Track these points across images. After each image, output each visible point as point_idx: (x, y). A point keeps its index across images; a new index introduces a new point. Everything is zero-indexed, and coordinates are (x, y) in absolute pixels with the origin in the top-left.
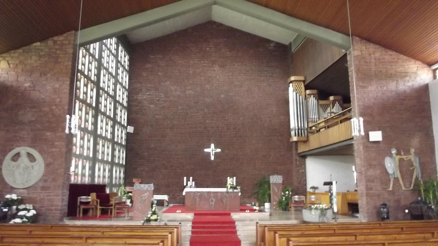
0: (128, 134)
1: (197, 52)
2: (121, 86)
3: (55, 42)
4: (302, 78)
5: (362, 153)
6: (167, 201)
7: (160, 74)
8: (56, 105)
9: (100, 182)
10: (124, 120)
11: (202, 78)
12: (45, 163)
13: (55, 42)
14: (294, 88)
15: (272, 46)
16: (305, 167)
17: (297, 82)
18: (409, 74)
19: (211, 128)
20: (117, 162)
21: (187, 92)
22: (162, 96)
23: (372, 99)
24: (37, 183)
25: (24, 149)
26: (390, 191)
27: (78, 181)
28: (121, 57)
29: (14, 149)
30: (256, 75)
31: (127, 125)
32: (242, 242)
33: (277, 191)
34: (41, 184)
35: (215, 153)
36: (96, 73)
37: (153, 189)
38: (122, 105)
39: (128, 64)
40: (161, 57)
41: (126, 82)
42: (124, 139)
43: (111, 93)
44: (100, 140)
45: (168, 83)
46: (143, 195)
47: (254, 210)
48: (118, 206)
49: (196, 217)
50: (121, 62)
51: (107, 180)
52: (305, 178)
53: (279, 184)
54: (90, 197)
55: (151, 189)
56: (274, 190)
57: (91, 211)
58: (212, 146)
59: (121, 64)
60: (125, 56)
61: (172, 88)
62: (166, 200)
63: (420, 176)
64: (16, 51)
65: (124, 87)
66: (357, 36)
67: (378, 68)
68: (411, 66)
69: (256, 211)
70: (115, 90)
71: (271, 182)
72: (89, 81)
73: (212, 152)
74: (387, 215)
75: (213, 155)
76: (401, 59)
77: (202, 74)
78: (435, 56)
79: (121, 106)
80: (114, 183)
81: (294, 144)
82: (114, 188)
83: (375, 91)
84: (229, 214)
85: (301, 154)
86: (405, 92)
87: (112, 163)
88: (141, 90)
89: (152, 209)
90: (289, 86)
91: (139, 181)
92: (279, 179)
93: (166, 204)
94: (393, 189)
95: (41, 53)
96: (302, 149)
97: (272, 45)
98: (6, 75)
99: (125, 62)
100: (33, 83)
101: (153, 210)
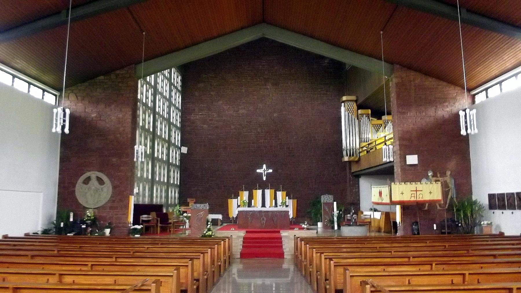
0: (182, 155)
1: (249, 70)
3: (117, 76)
6: (221, 221)
7: (212, 93)
8: (120, 134)
9: (162, 202)
13: (117, 76)
15: (326, 62)
18: (448, 100)
19: (264, 147)
21: (241, 112)
23: (411, 125)
24: (106, 203)
26: (426, 210)
30: (310, 92)
34: (109, 205)
36: (152, 99)
37: (208, 208)
38: (175, 126)
42: (178, 160)
43: (166, 116)
44: (157, 162)
49: (247, 234)
51: (163, 200)
54: (151, 216)
56: (325, 210)
57: (152, 229)
58: (264, 166)
59: (174, 86)
60: (177, 77)
61: (225, 107)
62: (220, 219)
66: (397, 64)
68: (450, 92)
69: (304, 229)
74: (418, 231)
76: (440, 85)
78: (477, 80)
80: (170, 203)
81: (348, 163)
84: (279, 232)
85: (355, 174)
87: (168, 184)
88: (194, 110)
92: (330, 199)
93: (219, 223)
95: (105, 86)
97: (326, 61)
98: (74, 107)
99: (177, 83)
101: (208, 227)
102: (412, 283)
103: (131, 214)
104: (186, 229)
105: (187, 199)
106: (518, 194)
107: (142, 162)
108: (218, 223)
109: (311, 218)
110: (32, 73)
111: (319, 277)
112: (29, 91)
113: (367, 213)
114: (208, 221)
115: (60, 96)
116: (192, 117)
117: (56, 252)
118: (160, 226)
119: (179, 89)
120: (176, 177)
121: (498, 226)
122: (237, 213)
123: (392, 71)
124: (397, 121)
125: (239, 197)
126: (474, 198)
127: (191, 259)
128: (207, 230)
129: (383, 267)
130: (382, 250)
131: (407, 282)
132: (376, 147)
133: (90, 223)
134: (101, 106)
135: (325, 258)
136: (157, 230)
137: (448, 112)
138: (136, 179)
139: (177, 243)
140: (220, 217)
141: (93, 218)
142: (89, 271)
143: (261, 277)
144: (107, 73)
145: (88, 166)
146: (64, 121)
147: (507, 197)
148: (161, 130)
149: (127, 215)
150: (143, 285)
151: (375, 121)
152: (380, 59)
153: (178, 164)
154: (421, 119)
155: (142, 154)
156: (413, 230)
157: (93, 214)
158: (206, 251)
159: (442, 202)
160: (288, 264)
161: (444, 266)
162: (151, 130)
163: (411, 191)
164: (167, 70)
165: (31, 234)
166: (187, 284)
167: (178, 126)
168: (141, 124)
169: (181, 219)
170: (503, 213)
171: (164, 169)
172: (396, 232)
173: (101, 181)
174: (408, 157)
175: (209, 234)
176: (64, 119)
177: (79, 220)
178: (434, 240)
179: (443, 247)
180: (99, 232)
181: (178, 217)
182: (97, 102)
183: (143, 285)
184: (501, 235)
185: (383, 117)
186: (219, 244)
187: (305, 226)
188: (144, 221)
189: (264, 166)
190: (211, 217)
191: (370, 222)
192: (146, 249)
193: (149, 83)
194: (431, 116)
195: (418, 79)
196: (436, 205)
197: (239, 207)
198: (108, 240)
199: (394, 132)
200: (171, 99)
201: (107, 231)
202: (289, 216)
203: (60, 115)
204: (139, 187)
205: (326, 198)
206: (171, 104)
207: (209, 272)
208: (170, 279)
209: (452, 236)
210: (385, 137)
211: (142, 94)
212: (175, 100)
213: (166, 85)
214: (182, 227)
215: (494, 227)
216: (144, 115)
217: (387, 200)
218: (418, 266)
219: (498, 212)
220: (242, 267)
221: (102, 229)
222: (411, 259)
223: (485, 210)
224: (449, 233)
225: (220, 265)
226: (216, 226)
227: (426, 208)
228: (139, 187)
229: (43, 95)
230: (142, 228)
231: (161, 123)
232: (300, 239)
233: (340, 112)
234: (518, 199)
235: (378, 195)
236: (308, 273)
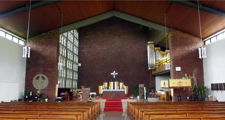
0: (79, 67)
6: (96, 95)
7: (92, 40)
8: (52, 58)
13: (51, 33)
21: (104, 48)
24: (45, 88)
25: (40, 75)
27: (60, 87)
28: (75, 34)
29: (36, 75)
31: (78, 63)
33: (142, 91)
34: (47, 88)
35: (115, 75)
37: (90, 90)
38: (76, 54)
51: (71, 86)
56: (140, 91)
57: (66, 99)
59: (75, 37)
60: (77, 33)
61: (97, 46)
64: (36, 36)
66: (172, 28)
70: (73, 49)
84: (121, 100)
85: (153, 75)
87: (73, 79)
88: (84, 47)
93: (95, 96)
94: (185, 90)
99: (77, 36)
104: (80, 99)
106: (224, 84)
107: (61, 70)
109: (134, 94)
112: (12, 40)
114: (90, 96)
115: (26, 42)
116: (83, 51)
117: (24, 109)
120: (76, 76)
121: (215, 98)
123: (170, 31)
125: (103, 85)
126: (205, 86)
127: (83, 112)
129: (166, 115)
134: (44, 46)
135: (141, 111)
138: (59, 77)
139: (77, 105)
140: (95, 93)
142: (38, 117)
144: (46, 32)
145: (38, 72)
146: (28, 52)
147: (219, 85)
148: (70, 56)
149: (55, 93)
151: (162, 52)
152: (164, 26)
156: (178, 99)
159: (191, 87)
160: (124, 114)
162: (65, 56)
165: (13, 101)
168: (61, 54)
169: (79, 94)
171: (71, 73)
172: (171, 100)
173: (43, 78)
177: (34, 95)
178: (188, 104)
179: (192, 107)
182: (42, 44)
184: (217, 101)
185: (166, 51)
186: (94, 105)
187: (132, 98)
190: (91, 93)
191: (160, 96)
193: (65, 36)
195: (181, 34)
199: (170, 57)
201: (46, 100)
202: (125, 93)
204: (60, 81)
205: (141, 86)
206: (74, 45)
210: (167, 59)
211: (61, 40)
212: (76, 43)
213: (72, 37)
214: (79, 98)
215: (213, 98)
217: (167, 86)
219: (215, 91)
221: (44, 99)
222: (178, 112)
225: (95, 114)
227: (184, 90)
228: (60, 81)
229: (19, 41)
230: (61, 98)
231: (70, 53)
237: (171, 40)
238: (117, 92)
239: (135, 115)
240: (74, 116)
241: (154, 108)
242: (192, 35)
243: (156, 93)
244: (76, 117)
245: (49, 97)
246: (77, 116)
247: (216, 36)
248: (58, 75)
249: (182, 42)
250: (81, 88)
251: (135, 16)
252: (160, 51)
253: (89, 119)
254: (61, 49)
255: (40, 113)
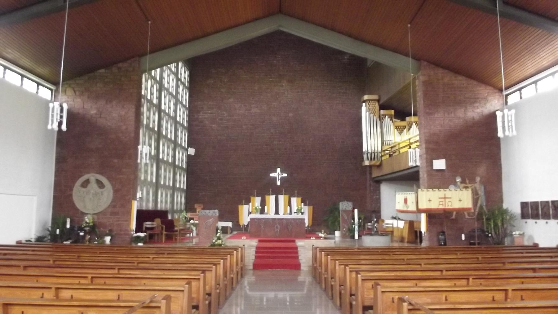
0: (189, 157)
2: (181, 105)
4: (375, 97)
5: (426, 181)
6: (231, 228)
7: (222, 90)
9: (167, 208)
10: (185, 141)
11: (269, 95)
12: (113, 189)
13: (119, 68)
14: (368, 108)
16: (380, 193)
17: (371, 102)
19: (278, 150)
20: (178, 186)
22: (225, 115)
24: (105, 209)
25: (93, 176)
26: (453, 219)
28: (181, 74)
32: (301, 265)
33: (346, 218)
34: (110, 210)
36: (158, 95)
37: (217, 214)
38: (182, 125)
39: (188, 80)
40: (223, 71)
41: (186, 100)
43: (172, 114)
45: (231, 100)
46: (208, 221)
47: (320, 238)
48: (182, 232)
50: (181, 79)
52: (379, 205)
53: (349, 211)
54: (155, 223)
55: (216, 215)
58: (279, 170)
59: (181, 82)
60: (185, 72)
61: (236, 105)
62: (230, 227)
63: (484, 204)
65: (185, 106)
66: (425, 60)
67: (446, 94)
70: (175, 111)
71: (341, 208)
72: (152, 105)
73: (278, 177)
75: (279, 180)
77: (269, 90)
79: (182, 127)
80: (175, 208)
81: (368, 169)
82: (175, 214)
83: (442, 118)
84: (294, 241)
86: (473, 118)
87: (174, 188)
88: (202, 108)
89: (217, 234)
90: (362, 106)
91: (201, 206)
93: (229, 231)
96: (376, 174)
99: (185, 78)
100: (99, 110)
101: (218, 235)
102: (449, 300)
103: (133, 220)
104: (193, 238)
105: (194, 205)
106: (553, 202)
107: (146, 164)
108: (227, 230)
109: (327, 227)
110: (24, 63)
111: (343, 292)
112: (22, 84)
113: (388, 222)
114: (217, 229)
115: (57, 91)
116: (201, 116)
117: (51, 262)
118: (165, 234)
119: (186, 85)
120: (182, 181)
121: (531, 237)
122: (249, 220)
123: (419, 69)
124: (423, 122)
125: (250, 204)
126: (505, 206)
127: (204, 272)
128: (216, 239)
129: (415, 282)
130: (411, 262)
131: (444, 298)
132: (411, 146)
133: (89, 230)
134: (102, 103)
135: (351, 271)
136: (162, 238)
137: (478, 114)
138: (139, 182)
139: (184, 252)
140: (229, 224)
141: (92, 224)
142: (88, 285)
143: (272, 290)
144: (107, 66)
145: (87, 168)
146: (61, 117)
147: (541, 205)
148: (167, 129)
149: (129, 221)
150: (151, 302)
151: (399, 123)
152: (407, 55)
153: (184, 167)
154: (449, 120)
155: (146, 154)
156: (439, 240)
157: (91, 221)
158: (219, 262)
159: (473, 211)
160: (305, 276)
161: (482, 280)
162: (156, 129)
163: (440, 198)
164: (173, 64)
165: (24, 242)
166: (199, 301)
167: (185, 125)
168: (145, 122)
169: (188, 226)
170: (536, 223)
171: (170, 172)
172: (421, 242)
173: (100, 185)
174: (435, 162)
175: (218, 243)
176: (62, 114)
177: (77, 227)
178: (464, 251)
179: (476, 259)
180: (99, 239)
181: (185, 225)
182: (97, 97)
183: (151, 302)
184: (536, 246)
185: (408, 119)
186: (231, 254)
187: (323, 236)
188: (147, 229)
189: (279, 170)
190: (221, 224)
191: (392, 232)
192: (151, 259)
193: (154, 78)
194: (460, 118)
195: (447, 77)
196: (464, 213)
197: (250, 214)
198: (465, 248)
199: (420, 135)
200: (177, 96)
201: (108, 239)
202: (304, 224)
203: (57, 110)
204: (142, 191)
205: (345, 206)
206: (177, 102)
207: (221, 286)
208: (181, 294)
209: (483, 246)
210: (410, 139)
211: (146, 89)
212: (182, 97)
213: (173, 80)
214: (188, 235)
215: (526, 238)
216: (148, 113)
217: (413, 208)
218: (452, 280)
219: (531, 222)
220: (254, 279)
221: (101, 237)
222: (445, 273)
223: (516, 219)
224: (479, 244)
225: (232, 278)
226: (226, 234)
227: (454, 217)
228: (142, 191)
229: (38, 89)
230: (145, 236)
231: (167, 122)
232: (320, 249)
233: (360, 113)
234: (553, 208)
235: (403, 201)
236: (330, 286)
237: (423, 91)
238: (285, 221)
239: (333, 279)
240: (183, 283)
241: (377, 262)
242: (474, 79)
243: (384, 224)
244: (187, 286)
245: (115, 232)
246: (191, 282)
247: (520, 90)
248: (136, 177)
249: (449, 97)
250: (193, 210)
251: (333, 29)
252: (394, 120)
253: (217, 289)
254: (145, 109)
255: (91, 274)
